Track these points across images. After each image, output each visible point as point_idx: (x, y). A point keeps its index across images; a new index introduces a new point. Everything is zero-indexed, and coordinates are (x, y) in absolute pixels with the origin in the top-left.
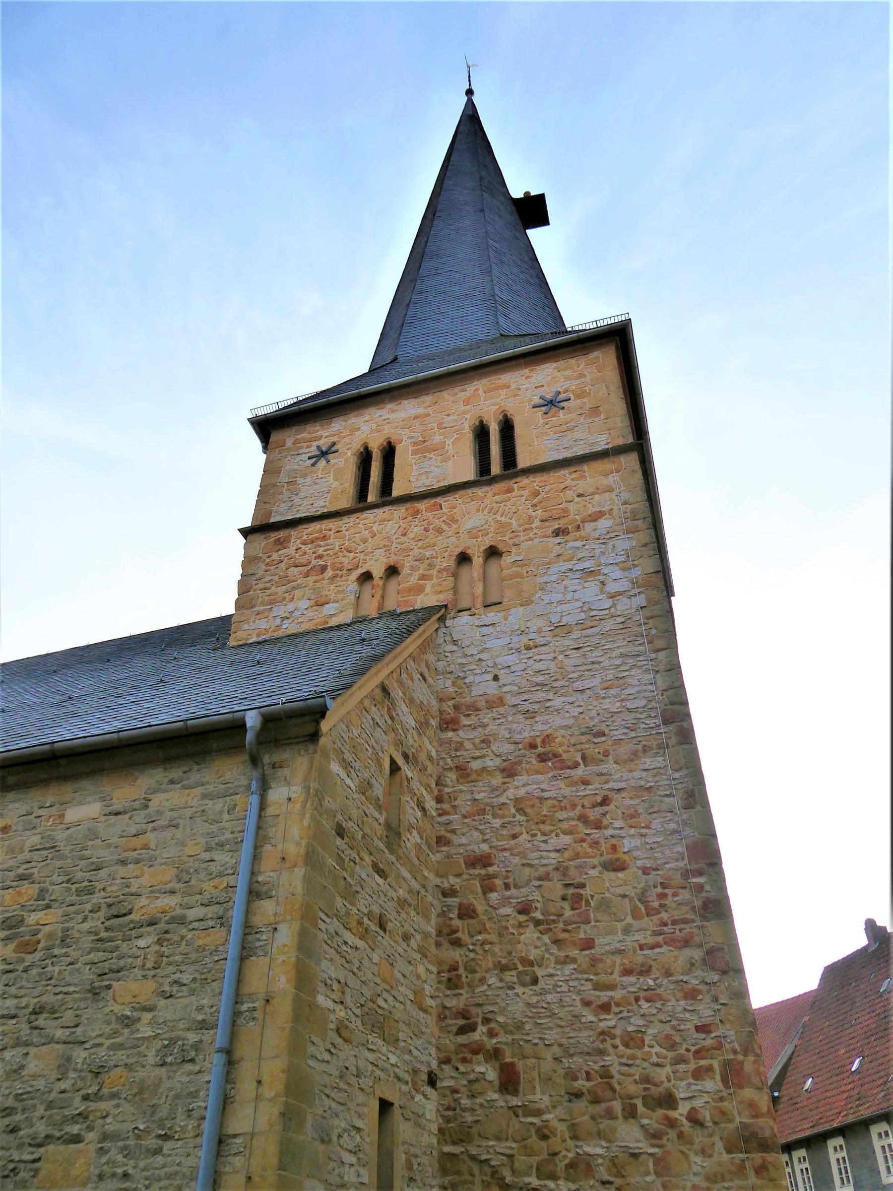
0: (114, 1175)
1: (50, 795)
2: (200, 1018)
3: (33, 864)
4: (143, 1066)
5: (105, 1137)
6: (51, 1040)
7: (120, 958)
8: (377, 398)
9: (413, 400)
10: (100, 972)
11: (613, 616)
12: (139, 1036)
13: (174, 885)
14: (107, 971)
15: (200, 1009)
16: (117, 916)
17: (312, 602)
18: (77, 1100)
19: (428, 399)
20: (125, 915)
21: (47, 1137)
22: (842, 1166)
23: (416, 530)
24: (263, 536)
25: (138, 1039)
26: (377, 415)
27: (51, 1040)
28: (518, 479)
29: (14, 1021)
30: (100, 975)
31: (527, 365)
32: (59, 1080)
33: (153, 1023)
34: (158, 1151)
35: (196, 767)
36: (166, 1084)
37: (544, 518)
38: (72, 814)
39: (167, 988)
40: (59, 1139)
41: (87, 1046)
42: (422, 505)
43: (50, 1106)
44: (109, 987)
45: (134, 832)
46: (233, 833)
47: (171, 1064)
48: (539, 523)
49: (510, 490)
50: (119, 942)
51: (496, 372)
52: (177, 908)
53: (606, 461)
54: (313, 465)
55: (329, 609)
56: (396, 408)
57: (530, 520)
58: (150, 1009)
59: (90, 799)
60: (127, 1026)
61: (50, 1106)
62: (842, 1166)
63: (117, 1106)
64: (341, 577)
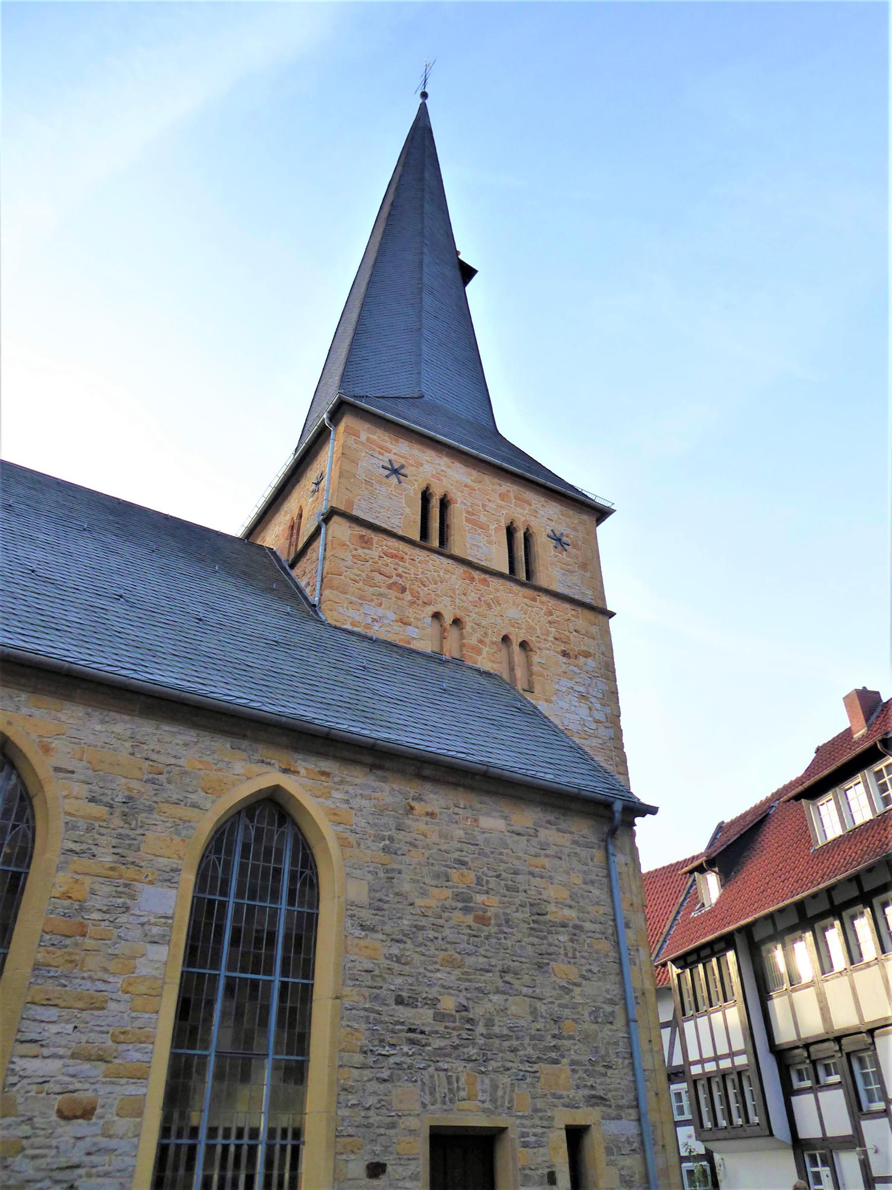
0: (585, 1086)
1: (474, 800)
2: (609, 997)
3: (464, 853)
4: (584, 1022)
5: (573, 1063)
6: (519, 994)
7: (550, 945)
8: (440, 447)
9: (463, 467)
10: (540, 952)
11: (596, 737)
12: (575, 1001)
13: (569, 902)
14: (544, 952)
15: (607, 991)
16: (539, 914)
17: (397, 617)
18: (549, 1037)
19: (475, 473)
20: (544, 915)
21: (538, 1058)
22: (229, 1174)
23: (473, 596)
24: (348, 524)
25: (576, 1003)
26: (436, 462)
27: (519, 994)
28: (541, 594)
29: (491, 974)
30: (540, 955)
31: (544, 495)
32: (533, 1021)
33: (582, 995)
34: (605, 1075)
35: (562, 817)
36: (600, 1035)
37: (557, 637)
38: (487, 822)
39: (585, 973)
40: (546, 1060)
41: (544, 1001)
42: (476, 575)
43: (532, 1038)
44: (548, 964)
45: (534, 854)
46: (597, 876)
47: (601, 1023)
48: (553, 639)
49: (534, 600)
50: (546, 934)
51: (525, 486)
52: (576, 919)
53: (592, 613)
54: (387, 477)
55: (411, 631)
56: (451, 464)
57: (548, 633)
58: (578, 985)
59: (494, 814)
60: (567, 994)
61: (532, 1038)
62: (229, 1174)
63: (575, 1044)
64: (418, 605)
